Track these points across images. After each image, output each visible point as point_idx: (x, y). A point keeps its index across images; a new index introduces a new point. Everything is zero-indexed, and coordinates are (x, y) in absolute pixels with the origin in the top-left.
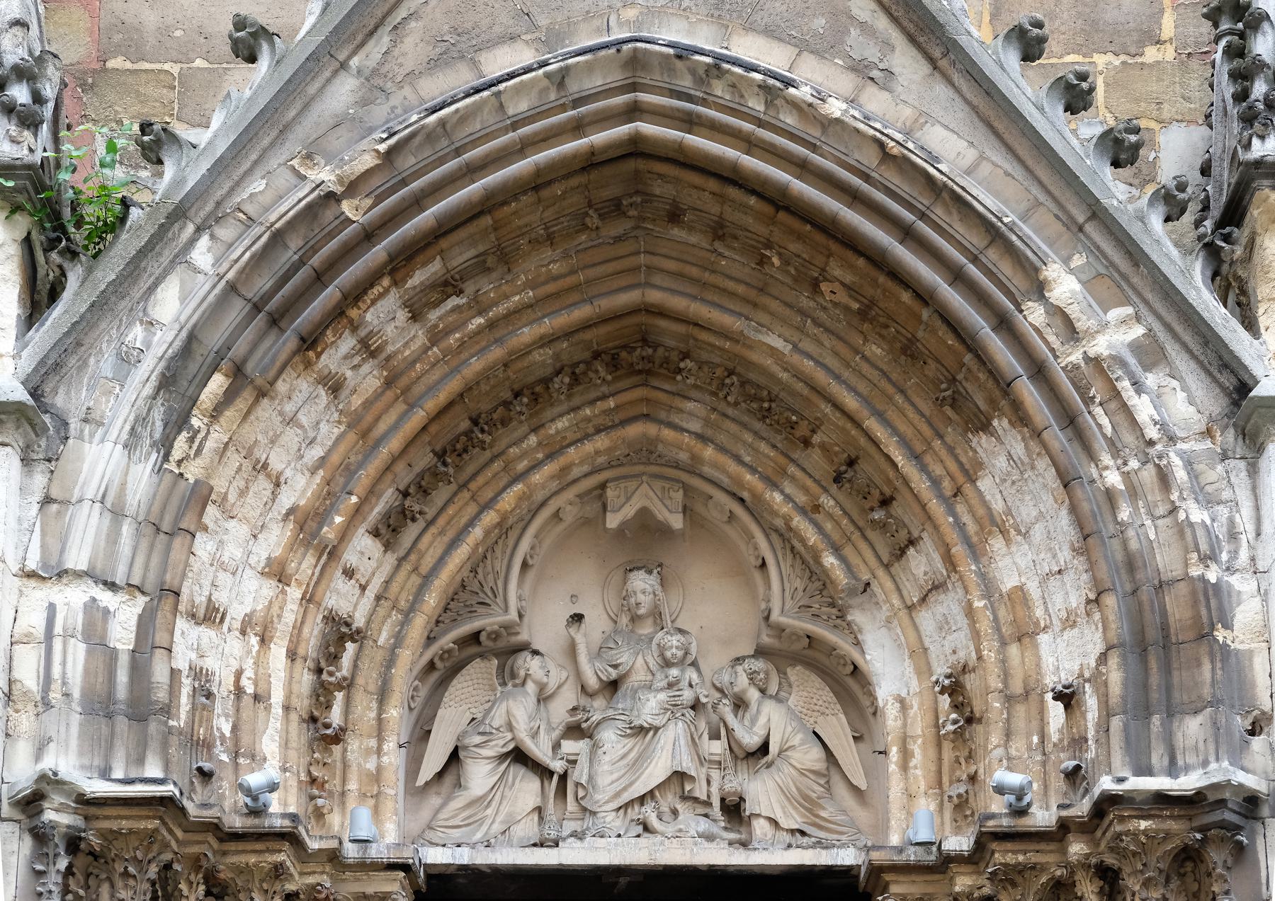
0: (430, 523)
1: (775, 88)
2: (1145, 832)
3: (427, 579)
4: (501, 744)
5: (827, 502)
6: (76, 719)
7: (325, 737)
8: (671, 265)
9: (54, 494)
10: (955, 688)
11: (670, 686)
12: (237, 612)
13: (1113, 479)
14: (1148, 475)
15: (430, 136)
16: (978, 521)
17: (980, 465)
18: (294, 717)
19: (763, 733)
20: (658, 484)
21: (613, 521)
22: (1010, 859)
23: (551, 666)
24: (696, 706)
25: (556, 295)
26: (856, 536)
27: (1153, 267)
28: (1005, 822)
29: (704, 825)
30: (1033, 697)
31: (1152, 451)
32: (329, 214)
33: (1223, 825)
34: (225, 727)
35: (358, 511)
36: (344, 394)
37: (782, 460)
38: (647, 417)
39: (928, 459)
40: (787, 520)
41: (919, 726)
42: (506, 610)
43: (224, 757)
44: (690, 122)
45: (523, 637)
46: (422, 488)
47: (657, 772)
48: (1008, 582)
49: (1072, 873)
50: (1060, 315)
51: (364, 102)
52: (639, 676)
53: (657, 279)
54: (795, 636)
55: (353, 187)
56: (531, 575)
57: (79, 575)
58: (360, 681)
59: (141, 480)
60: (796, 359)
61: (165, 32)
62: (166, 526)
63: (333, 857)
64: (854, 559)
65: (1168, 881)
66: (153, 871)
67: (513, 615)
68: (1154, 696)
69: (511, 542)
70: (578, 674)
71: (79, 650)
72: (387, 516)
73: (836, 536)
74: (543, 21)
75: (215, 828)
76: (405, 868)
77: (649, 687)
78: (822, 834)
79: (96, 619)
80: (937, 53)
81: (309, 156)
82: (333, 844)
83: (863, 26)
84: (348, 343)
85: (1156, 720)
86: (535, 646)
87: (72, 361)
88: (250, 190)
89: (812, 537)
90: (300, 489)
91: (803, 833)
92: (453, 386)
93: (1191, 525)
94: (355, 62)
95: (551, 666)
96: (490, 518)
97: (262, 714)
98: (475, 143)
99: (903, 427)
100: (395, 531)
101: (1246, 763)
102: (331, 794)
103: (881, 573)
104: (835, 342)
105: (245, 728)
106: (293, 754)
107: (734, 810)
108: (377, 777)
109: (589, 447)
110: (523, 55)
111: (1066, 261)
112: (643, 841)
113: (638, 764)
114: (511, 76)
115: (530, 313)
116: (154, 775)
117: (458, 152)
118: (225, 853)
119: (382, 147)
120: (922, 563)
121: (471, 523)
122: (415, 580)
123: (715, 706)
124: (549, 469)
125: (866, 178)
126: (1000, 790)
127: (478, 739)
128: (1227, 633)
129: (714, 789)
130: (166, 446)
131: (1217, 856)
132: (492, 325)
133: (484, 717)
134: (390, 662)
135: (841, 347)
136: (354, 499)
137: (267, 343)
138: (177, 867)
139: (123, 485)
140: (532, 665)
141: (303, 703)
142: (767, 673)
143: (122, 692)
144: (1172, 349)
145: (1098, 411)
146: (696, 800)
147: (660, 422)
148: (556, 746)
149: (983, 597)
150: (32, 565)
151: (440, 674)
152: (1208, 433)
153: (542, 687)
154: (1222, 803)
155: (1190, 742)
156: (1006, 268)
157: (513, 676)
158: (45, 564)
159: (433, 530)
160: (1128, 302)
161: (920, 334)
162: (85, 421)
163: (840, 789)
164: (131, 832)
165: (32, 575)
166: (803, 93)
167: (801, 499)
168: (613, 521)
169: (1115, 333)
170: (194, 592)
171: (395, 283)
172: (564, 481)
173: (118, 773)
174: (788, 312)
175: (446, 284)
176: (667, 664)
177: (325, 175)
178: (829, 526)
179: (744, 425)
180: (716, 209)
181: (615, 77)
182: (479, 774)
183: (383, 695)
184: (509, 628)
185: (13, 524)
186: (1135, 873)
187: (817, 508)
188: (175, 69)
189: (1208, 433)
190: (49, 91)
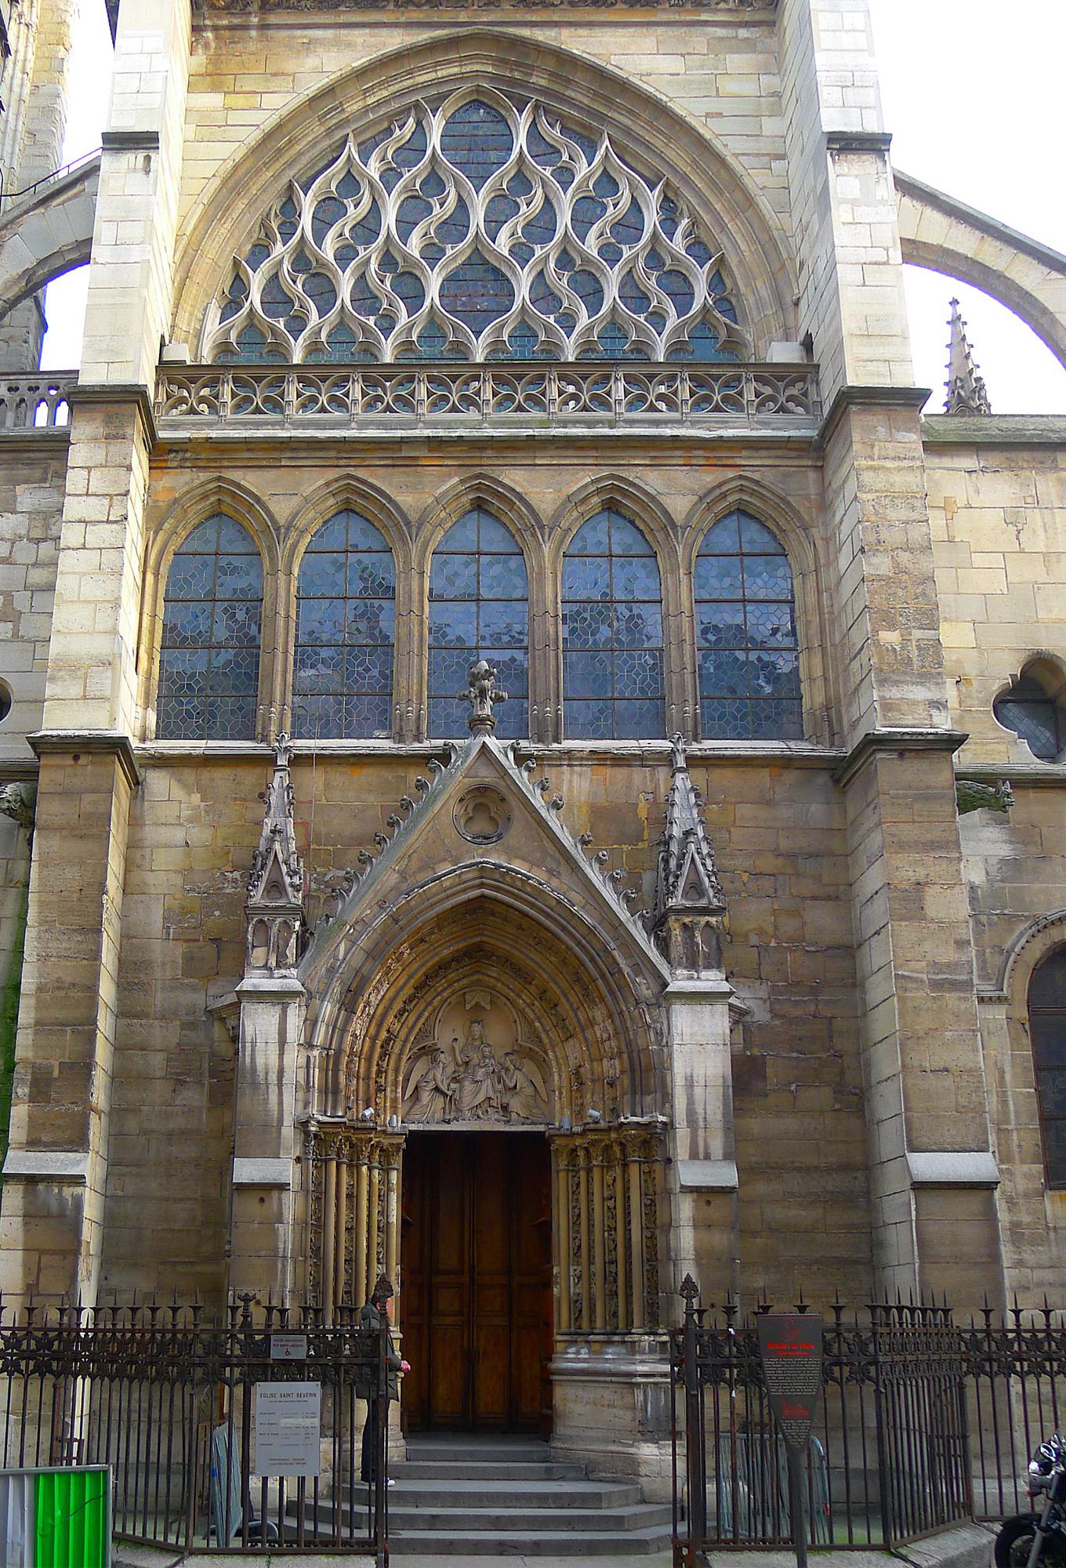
4: (432, 1085)
21: (468, 1007)
47: (481, 1097)
52: (475, 1061)
107: (505, 1108)
124: (449, 991)
151: (414, 1059)
163: (539, 1100)
176: (484, 1057)
182: (426, 1097)
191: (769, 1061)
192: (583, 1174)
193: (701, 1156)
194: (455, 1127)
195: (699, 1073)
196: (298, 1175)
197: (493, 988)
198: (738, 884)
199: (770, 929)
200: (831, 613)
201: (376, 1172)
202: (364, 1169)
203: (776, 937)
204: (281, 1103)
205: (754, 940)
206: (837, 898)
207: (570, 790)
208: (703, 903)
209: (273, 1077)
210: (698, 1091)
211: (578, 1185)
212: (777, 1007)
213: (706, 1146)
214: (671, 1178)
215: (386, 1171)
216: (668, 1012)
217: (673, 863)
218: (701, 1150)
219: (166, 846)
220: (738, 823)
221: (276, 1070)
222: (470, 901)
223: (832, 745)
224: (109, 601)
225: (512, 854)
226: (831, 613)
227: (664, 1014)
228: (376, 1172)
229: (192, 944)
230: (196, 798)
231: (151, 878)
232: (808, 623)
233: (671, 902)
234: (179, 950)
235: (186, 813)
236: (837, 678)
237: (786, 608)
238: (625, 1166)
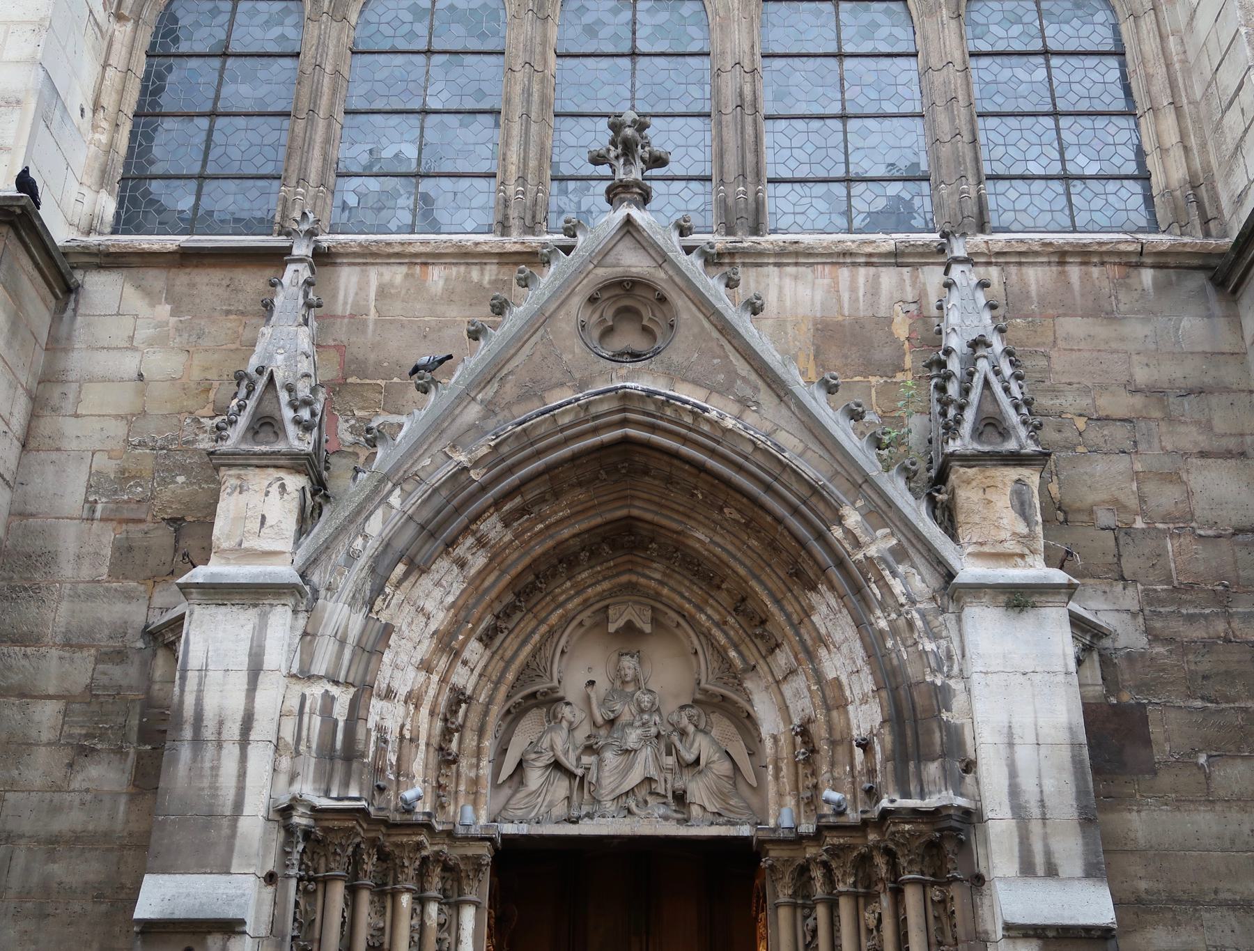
0: (510, 632)
1: (698, 413)
2: (908, 831)
3: (509, 663)
4: (546, 759)
5: (731, 620)
6: (313, 761)
7: (447, 760)
8: (645, 496)
9: (309, 631)
10: (804, 731)
11: (644, 724)
12: (403, 692)
13: (883, 624)
14: (902, 622)
15: (517, 436)
16: (812, 639)
17: (812, 608)
18: (431, 750)
19: (696, 753)
20: (637, 607)
22: (836, 841)
23: (577, 712)
24: (658, 736)
25: (583, 511)
26: (747, 640)
27: (899, 510)
28: (832, 819)
29: (662, 810)
30: (846, 743)
31: (903, 609)
32: (463, 477)
33: (951, 828)
34: (393, 758)
35: (473, 630)
36: (466, 568)
37: (706, 596)
38: (630, 570)
39: (785, 602)
40: (709, 630)
41: (785, 752)
42: (552, 680)
43: (392, 777)
44: (653, 428)
45: (561, 694)
46: (508, 612)
47: (635, 777)
48: (831, 675)
49: (871, 851)
50: (848, 532)
51: (485, 418)
52: (626, 718)
53: (637, 503)
54: (714, 695)
55: (476, 464)
56: (566, 657)
57: (320, 678)
58: (468, 724)
59: (357, 622)
60: (712, 547)
61: (379, 363)
62: (368, 648)
63: (450, 835)
64: (746, 653)
65: (923, 857)
66: (350, 849)
67: (555, 683)
68: (910, 750)
69: (555, 640)
70: (591, 714)
71: (317, 721)
72: (487, 629)
73: (736, 639)
74: (577, 376)
75: (385, 822)
76: (490, 839)
77: (631, 725)
78: (732, 815)
79: (328, 700)
80: (782, 394)
81: (454, 446)
82: (450, 827)
83: (743, 378)
84: (470, 541)
85: (912, 765)
86: (568, 699)
87: (324, 557)
88: (423, 464)
89: (723, 640)
90: (440, 619)
91: (720, 815)
92: (527, 560)
93: (926, 652)
94: (479, 397)
95: (577, 712)
96: (544, 628)
97: (414, 750)
98: (541, 439)
99: (770, 585)
100: (491, 638)
101: (964, 791)
102: (449, 793)
103: (761, 661)
104: (733, 538)
105: (404, 758)
106: (430, 772)
107: (680, 798)
108: (475, 782)
109: (599, 588)
110: (566, 395)
111: (853, 503)
112: (628, 820)
113: (629, 768)
114: (561, 406)
115: (566, 522)
116: (355, 794)
117: (532, 444)
118: (389, 835)
119: (492, 444)
120: (783, 659)
121: (533, 632)
122: (502, 664)
123: (669, 736)
124: (577, 601)
125: (746, 458)
126: (827, 801)
127: (533, 756)
128: (949, 714)
129: (669, 786)
130: (371, 604)
131: (949, 846)
132: (547, 527)
133: (538, 741)
134: (486, 713)
135: (737, 542)
136: (470, 625)
137: (427, 546)
138: (363, 846)
139: (347, 626)
140: (566, 711)
141: (435, 741)
142: (699, 716)
143: (339, 745)
144: (911, 551)
145: (873, 586)
146: (658, 794)
147: (638, 574)
148: (579, 759)
149: (816, 684)
150: (294, 670)
151: (514, 715)
152: (934, 599)
153: (571, 723)
154: (949, 816)
155: (931, 778)
156: (821, 507)
157: (555, 717)
158: (301, 671)
159: (512, 636)
160: (887, 526)
161: (778, 537)
162: (328, 589)
164: (340, 829)
165: (294, 676)
166: (713, 415)
167: (716, 617)
168: (612, 628)
169: (879, 544)
170: (381, 683)
171: (497, 510)
172: (586, 604)
173: (334, 794)
174: (707, 522)
175: (523, 509)
176: (642, 711)
177: (462, 458)
178: (732, 633)
179: (685, 577)
180: (668, 469)
181: (615, 405)
182: (535, 778)
183: (481, 732)
184: (553, 690)
185: (286, 647)
186: (904, 856)
187: (725, 623)
188: (382, 383)
189: (934, 599)
190: (319, 411)
191: (1153, 714)
192: (821, 912)
193: (1040, 870)
194: (587, 828)
195: (1024, 721)
196: (267, 909)
197: (657, 596)
198: (1069, 434)
199: (1133, 503)
200: (1184, 61)
201: (433, 909)
202: (405, 900)
203: (1143, 514)
204: (242, 775)
205: (1104, 518)
206: (1243, 454)
207: (780, 298)
208: (1011, 445)
209: (233, 730)
210: (1024, 755)
211: (814, 932)
212: (1158, 624)
213: (1048, 854)
214: (984, 912)
215: (453, 904)
216: (959, 620)
217: (953, 389)
218: (1039, 860)
219: (105, 380)
220: (1061, 344)
221: (239, 716)
222: (603, 447)
223: (1207, 234)
224: (31, 22)
225: (674, 374)
226: (1184, 61)
227: (952, 624)
228: (433, 909)
229: (131, 527)
230: (164, 310)
231: (70, 427)
232: (1149, 77)
233: (954, 446)
234: (106, 538)
235: (143, 333)
236: (1203, 146)
237: (1113, 62)
238: (897, 894)
